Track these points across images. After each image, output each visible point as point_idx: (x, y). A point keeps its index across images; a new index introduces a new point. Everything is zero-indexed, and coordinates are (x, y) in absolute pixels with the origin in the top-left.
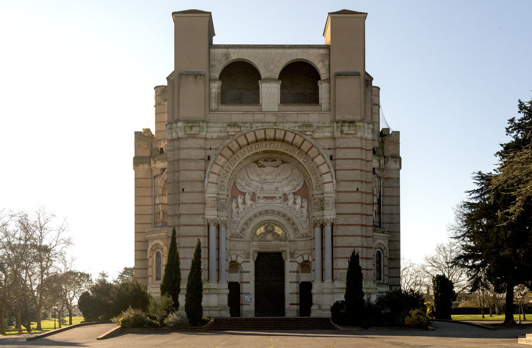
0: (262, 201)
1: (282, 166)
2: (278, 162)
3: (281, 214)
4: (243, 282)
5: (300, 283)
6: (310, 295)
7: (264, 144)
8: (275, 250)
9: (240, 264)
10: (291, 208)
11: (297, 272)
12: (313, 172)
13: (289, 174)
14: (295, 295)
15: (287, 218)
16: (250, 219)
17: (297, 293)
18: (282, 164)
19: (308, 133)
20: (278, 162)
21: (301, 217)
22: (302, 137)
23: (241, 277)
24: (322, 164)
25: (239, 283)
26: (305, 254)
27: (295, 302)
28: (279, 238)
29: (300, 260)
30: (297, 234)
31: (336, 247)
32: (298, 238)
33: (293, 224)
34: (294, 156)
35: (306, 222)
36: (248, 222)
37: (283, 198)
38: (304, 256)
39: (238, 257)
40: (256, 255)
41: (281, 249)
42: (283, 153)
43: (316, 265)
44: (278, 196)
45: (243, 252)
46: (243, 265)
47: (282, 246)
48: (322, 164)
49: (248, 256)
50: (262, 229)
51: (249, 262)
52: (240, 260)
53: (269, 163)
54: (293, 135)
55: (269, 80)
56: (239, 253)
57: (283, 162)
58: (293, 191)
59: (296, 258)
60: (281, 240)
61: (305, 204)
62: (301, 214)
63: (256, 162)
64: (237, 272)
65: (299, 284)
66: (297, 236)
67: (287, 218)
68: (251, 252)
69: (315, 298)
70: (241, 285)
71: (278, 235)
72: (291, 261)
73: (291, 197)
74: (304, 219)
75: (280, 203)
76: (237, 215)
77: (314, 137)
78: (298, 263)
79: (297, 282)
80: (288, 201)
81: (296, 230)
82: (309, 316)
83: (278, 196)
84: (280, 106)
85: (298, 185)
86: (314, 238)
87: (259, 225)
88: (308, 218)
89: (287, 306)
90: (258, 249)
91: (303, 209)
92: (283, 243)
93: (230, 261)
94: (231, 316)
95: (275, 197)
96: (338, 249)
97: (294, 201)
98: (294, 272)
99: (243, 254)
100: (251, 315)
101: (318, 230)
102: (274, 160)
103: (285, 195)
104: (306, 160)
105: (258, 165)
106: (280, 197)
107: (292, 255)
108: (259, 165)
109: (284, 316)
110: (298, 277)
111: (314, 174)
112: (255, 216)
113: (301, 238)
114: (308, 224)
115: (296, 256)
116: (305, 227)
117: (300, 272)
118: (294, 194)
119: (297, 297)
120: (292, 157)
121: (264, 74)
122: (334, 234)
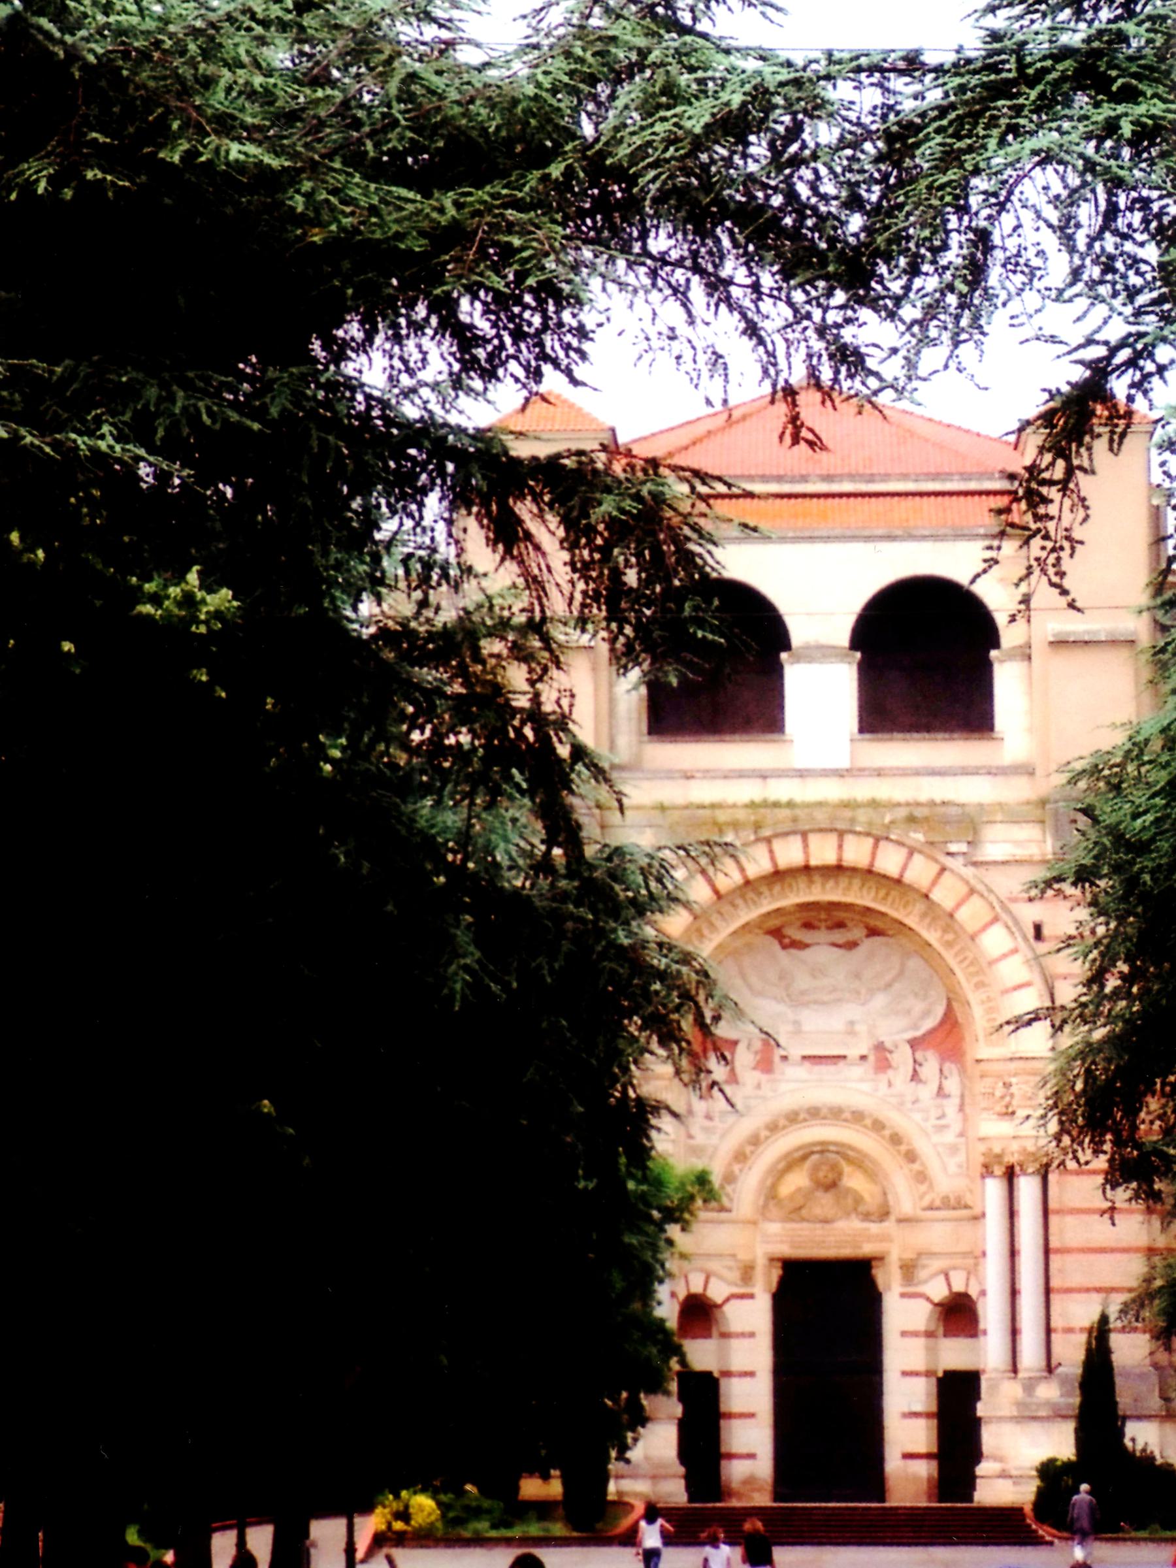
0: (802, 1072)
1: (868, 944)
2: (857, 933)
3: (868, 1122)
4: (727, 1374)
5: (940, 1374)
6: (974, 1425)
7: (802, 881)
8: (846, 1252)
9: (719, 1306)
10: (901, 1095)
11: (929, 1334)
12: (976, 979)
13: (894, 973)
14: (922, 1423)
15: (887, 1133)
16: (755, 1141)
17: (928, 1415)
18: (868, 936)
19: (953, 848)
20: (857, 933)
21: (942, 1128)
22: (936, 861)
23: (723, 1354)
24: (1004, 956)
25: (716, 1374)
26: (955, 1268)
27: (923, 1449)
28: (861, 1209)
29: (938, 1291)
30: (925, 1194)
31: (1059, 1251)
32: (931, 1208)
33: (911, 1157)
34: (907, 921)
35: (953, 1149)
36: (748, 1149)
37: (872, 1058)
38: (952, 1274)
39: (713, 1280)
40: (776, 1273)
41: (867, 1249)
42: (868, 909)
43: (992, 1313)
44: (853, 1052)
45: (731, 1263)
46: (727, 1308)
47: (870, 1239)
48: (1004, 956)
49: (747, 1273)
50: (798, 1180)
51: (751, 1296)
52: (717, 1292)
53: (822, 936)
54: (903, 852)
55: (821, 653)
56: (714, 1265)
57: (873, 932)
58: (910, 1035)
59: (925, 1282)
60: (867, 1217)
61: (952, 1085)
62: (939, 1118)
63: (777, 933)
64: (708, 1335)
65: (934, 1381)
66: (926, 1202)
67: (887, 1133)
68: (761, 1262)
69: (989, 1438)
70: (723, 1383)
71: (858, 1200)
72: (903, 1295)
73: (903, 1057)
74: (950, 1137)
75: (861, 1080)
76: (707, 1123)
77: (974, 859)
78: (928, 1299)
79: (928, 1374)
80: (890, 1073)
81: (922, 1177)
82: (971, 1500)
83: (853, 1052)
84: (859, 745)
85: (926, 1014)
86: (984, 1215)
87: (793, 1161)
88: (961, 1134)
89: (893, 1464)
90: (787, 1250)
91: (945, 1102)
92: (874, 1228)
93: (682, 1295)
94: (690, 1500)
95: (844, 1057)
96: (1070, 1259)
97: (915, 1071)
98: (915, 1334)
99: (730, 1268)
100: (763, 1499)
101: (994, 1189)
102: (840, 925)
103: (880, 1047)
104: (950, 937)
105: (781, 943)
106: (863, 1058)
107: (909, 1270)
108: (787, 941)
109: (882, 1499)
110: (931, 1351)
111: (980, 985)
112: (773, 1128)
113: (938, 1209)
114: (961, 1157)
115: (922, 1274)
116: (952, 1168)
117: (941, 1331)
118: (914, 1044)
119: (928, 1428)
120: (901, 923)
121: (798, 634)
122: (1052, 1205)
